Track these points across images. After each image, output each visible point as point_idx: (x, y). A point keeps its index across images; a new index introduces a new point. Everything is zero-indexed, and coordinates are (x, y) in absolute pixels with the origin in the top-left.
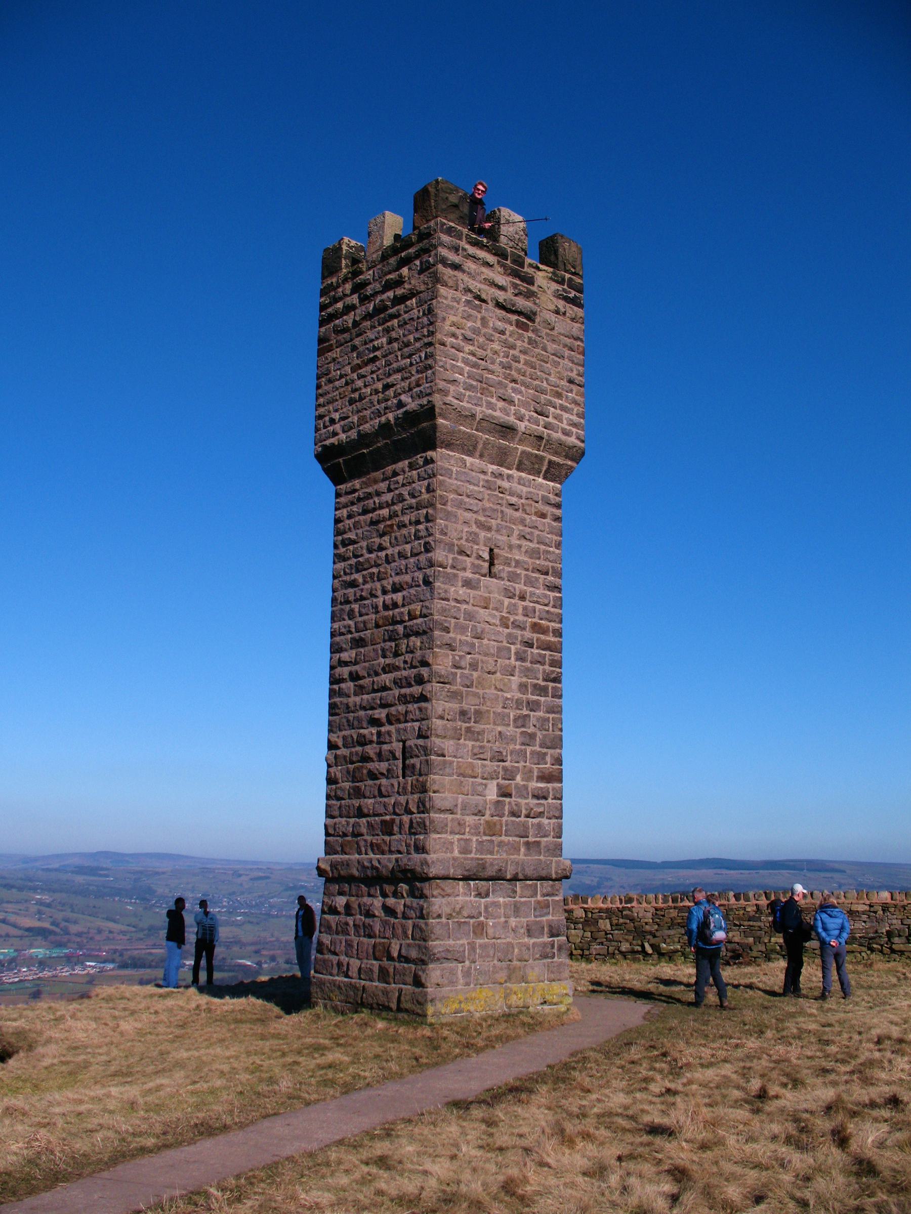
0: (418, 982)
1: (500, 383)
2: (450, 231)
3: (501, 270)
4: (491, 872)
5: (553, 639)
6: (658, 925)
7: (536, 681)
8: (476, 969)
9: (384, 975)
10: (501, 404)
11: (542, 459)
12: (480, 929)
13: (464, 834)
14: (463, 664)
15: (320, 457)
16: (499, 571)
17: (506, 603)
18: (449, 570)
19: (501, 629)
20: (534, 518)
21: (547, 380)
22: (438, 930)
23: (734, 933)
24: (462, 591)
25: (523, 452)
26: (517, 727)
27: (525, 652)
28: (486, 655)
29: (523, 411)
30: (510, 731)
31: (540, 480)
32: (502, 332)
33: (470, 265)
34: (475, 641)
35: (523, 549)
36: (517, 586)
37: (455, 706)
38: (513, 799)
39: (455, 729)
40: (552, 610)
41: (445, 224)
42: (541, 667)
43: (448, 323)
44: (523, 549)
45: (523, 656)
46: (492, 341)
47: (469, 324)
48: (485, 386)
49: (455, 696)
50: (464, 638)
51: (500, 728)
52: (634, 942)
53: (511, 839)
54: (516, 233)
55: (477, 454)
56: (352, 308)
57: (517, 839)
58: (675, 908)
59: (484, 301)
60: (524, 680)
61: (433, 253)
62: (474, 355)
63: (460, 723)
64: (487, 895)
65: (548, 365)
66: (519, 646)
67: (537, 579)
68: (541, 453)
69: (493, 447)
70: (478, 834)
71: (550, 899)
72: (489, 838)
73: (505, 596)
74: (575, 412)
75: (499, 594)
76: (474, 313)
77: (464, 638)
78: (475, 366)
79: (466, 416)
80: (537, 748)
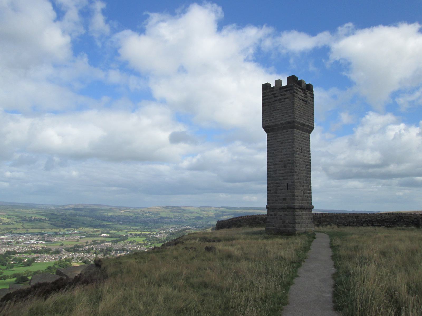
0: (294, 227)
2: (296, 86)
9: (285, 226)
10: (303, 120)
11: (308, 129)
12: (302, 218)
15: (263, 127)
18: (296, 152)
22: (297, 218)
24: (298, 156)
30: (304, 181)
31: (307, 134)
32: (303, 105)
33: (299, 93)
49: (297, 175)
78: (299, 113)
80: (308, 185)
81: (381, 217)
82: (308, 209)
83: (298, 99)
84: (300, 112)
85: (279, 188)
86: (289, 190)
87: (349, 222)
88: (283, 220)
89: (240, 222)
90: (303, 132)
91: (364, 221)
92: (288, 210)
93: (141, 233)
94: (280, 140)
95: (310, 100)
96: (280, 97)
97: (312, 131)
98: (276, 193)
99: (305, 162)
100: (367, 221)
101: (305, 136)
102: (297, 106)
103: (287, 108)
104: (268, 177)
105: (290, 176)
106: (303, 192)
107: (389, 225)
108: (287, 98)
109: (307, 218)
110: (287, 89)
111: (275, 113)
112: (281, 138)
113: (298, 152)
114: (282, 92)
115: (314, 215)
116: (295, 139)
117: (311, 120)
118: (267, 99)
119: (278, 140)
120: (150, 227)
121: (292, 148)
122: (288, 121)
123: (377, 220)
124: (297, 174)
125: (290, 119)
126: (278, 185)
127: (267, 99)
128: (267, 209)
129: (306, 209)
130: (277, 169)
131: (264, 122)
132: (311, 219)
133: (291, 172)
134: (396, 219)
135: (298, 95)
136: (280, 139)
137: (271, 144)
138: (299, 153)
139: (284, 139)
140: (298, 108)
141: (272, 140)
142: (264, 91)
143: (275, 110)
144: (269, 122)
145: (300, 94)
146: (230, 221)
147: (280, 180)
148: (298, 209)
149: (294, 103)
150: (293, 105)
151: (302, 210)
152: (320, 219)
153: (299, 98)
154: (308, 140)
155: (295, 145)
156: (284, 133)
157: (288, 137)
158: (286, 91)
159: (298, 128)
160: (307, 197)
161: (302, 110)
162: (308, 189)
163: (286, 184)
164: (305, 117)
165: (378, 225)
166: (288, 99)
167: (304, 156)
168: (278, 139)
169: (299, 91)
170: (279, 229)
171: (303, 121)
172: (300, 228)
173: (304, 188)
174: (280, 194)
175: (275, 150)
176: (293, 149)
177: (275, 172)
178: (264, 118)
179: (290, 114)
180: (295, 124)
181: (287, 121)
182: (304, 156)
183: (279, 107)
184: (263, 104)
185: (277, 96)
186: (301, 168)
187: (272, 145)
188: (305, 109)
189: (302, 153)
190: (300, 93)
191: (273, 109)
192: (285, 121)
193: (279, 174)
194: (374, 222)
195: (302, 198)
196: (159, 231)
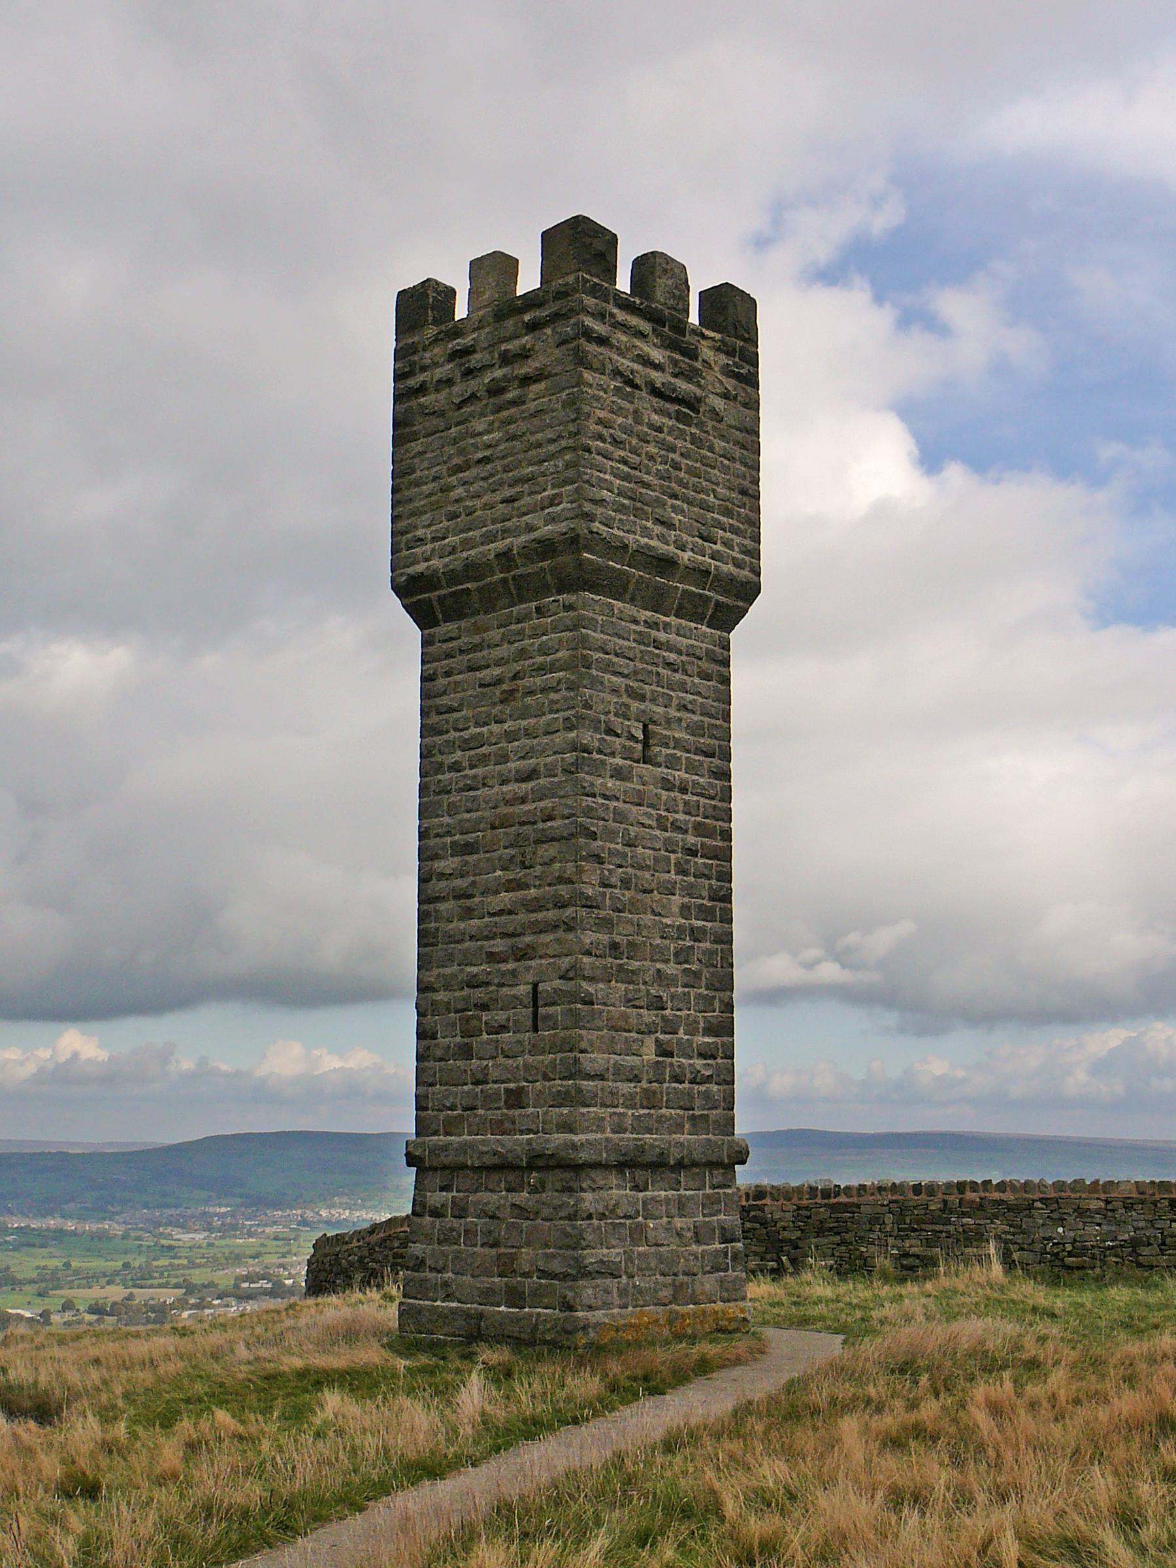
1: (657, 500)
4: (648, 1158)
5: (720, 844)
6: (802, 1231)
7: (701, 901)
8: (634, 1286)
9: (515, 1297)
10: (658, 529)
12: (638, 1234)
13: (617, 1107)
14: (613, 880)
15: (397, 589)
16: (656, 755)
17: (664, 798)
18: (595, 756)
19: (658, 833)
20: (697, 680)
21: (714, 491)
22: (589, 1237)
23: (913, 1242)
25: (685, 592)
26: (680, 963)
28: (641, 868)
29: (685, 537)
30: (671, 969)
32: (660, 430)
33: (622, 338)
34: (627, 849)
35: (684, 724)
36: (677, 773)
37: (604, 938)
38: (676, 1058)
39: (605, 967)
40: (719, 804)
41: (588, 281)
44: (684, 724)
45: (685, 867)
46: (648, 442)
47: (620, 420)
48: (639, 505)
49: (606, 924)
50: (613, 846)
51: (659, 966)
52: (768, 1257)
53: (673, 1112)
54: (676, 288)
56: (449, 382)
57: (681, 1112)
58: (825, 1205)
59: (637, 387)
60: (686, 900)
62: (625, 463)
63: (610, 960)
64: (646, 1189)
65: (716, 471)
66: (680, 855)
67: (701, 763)
68: (707, 593)
69: (647, 587)
70: (633, 1107)
71: (721, 1191)
72: (646, 1111)
73: (663, 788)
74: (748, 535)
76: (625, 404)
77: (613, 846)
78: (626, 478)
79: (616, 547)
80: (703, 991)
82: (695, 1164)
85: (485, 1016)
87: (1135, 1243)
88: (503, 1250)
93: (131, 1297)
94: (497, 671)
95: (726, 396)
96: (499, 373)
98: (466, 1052)
99: (677, 827)
102: (600, 428)
106: (657, 1040)
110: (543, 313)
112: (499, 662)
113: (613, 754)
118: (422, 389)
120: (185, 1262)
122: (537, 534)
125: (552, 519)
126: (479, 994)
127: (422, 389)
129: (680, 1165)
130: (474, 883)
136: (499, 662)
137: (445, 701)
139: (517, 667)
140: (616, 442)
146: (375, 1238)
147: (492, 957)
148: (597, 1165)
149: (578, 411)
151: (640, 1175)
158: (534, 327)
159: (617, 587)
161: (651, 458)
163: (523, 990)
169: (624, 327)
171: (662, 538)
173: (667, 1012)
175: (466, 745)
176: (573, 735)
179: (554, 486)
181: (532, 536)
187: (451, 710)
196: (236, 1286)
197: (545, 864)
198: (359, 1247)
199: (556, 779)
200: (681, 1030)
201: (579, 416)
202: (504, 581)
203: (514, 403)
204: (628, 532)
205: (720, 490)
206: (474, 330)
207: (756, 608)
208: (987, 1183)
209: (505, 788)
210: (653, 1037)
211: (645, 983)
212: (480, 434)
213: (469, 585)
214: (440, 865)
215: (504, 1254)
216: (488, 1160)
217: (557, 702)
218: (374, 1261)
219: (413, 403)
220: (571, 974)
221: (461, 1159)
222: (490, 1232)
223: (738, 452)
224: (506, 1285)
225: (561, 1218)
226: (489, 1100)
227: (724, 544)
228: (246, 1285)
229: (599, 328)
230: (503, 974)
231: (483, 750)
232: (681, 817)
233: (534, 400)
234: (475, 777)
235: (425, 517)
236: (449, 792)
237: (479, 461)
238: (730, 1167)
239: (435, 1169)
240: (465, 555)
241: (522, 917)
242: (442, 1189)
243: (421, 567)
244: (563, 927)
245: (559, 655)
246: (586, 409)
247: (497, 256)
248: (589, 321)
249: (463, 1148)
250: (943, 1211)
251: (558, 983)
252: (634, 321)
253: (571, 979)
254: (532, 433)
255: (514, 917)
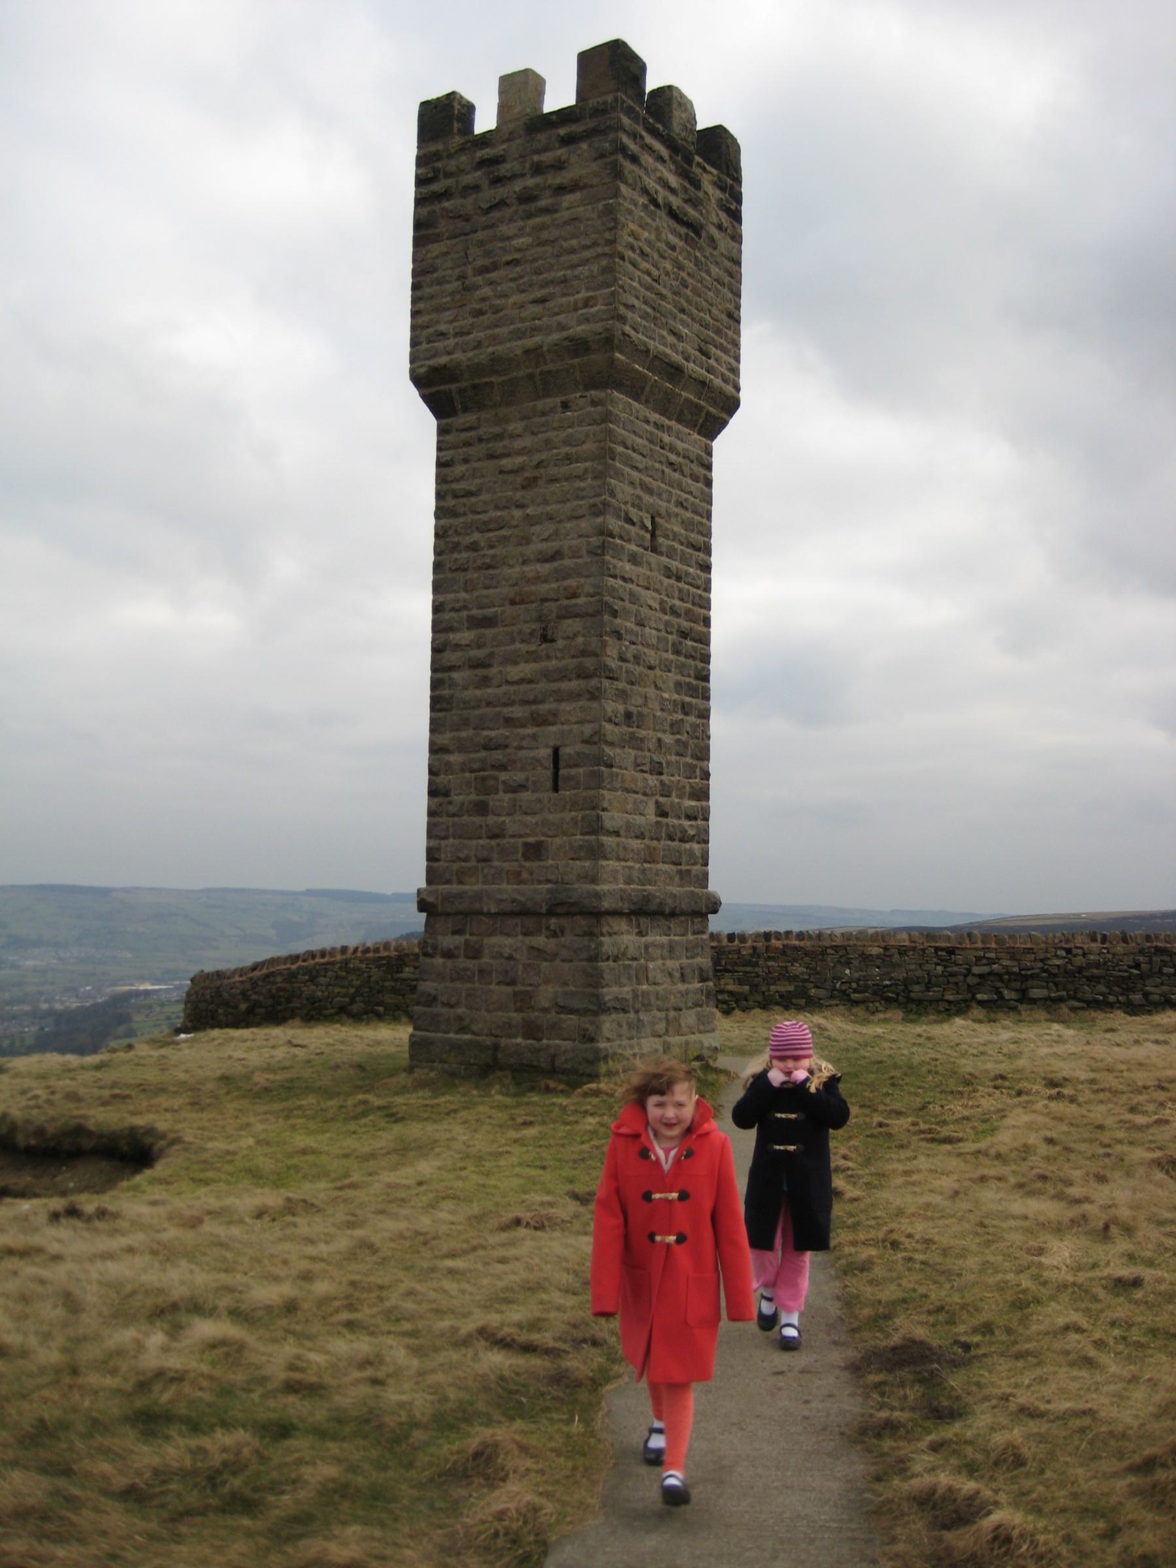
3: (672, 167)
9: (531, 1030)
10: (671, 339)
11: (699, 408)
12: (642, 975)
15: (419, 380)
18: (618, 541)
19: (661, 615)
20: (690, 481)
22: (608, 976)
24: (628, 567)
25: (686, 400)
27: (681, 643)
30: (668, 739)
31: (696, 436)
32: (673, 248)
33: (647, 159)
42: (693, 663)
43: (626, 231)
49: (623, 695)
51: (660, 735)
55: (643, 398)
61: (611, 137)
62: (649, 274)
75: (659, 570)
78: (649, 288)
80: (689, 760)
81: (1069, 951)
82: (682, 913)
83: (643, 200)
84: (655, 284)
85: (503, 776)
86: (566, 793)
87: (906, 982)
88: (519, 988)
89: (312, 980)
90: (667, 422)
91: (981, 976)
92: (553, 921)
94: (519, 460)
95: (720, 227)
96: (530, 182)
97: (724, 424)
98: (482, 809)
99: (674, 612)
100: (999, 976)
101: (680, 446)
102: (631, 240)
103: (573, 251)
104: (437, 703)
105: (575, 696)
106: (657, 802)
107: (1103, 994)
108: (574, 187)
109: (677, 975)
111: (491, 283)
112: (520, 452)
113: (629, 541)
114: (538, 152)
115: (725, 942)
116: (613, 459)
117: (725, 350)
118: (446, 194)
119: (506, 463)
121: (598, 510)
122: (571, 332)
123: (1045, 971)
124: (621, 685)
126: (497, 756)
127: (446, 194)
128: (425, 914)
129: (673, 914)
130: (491, 655)
131: (425, 346)
132: (703, 979)
133: (583, 674)
134: (1137, 966)
135: (647, 174)
136: (520, 452)
138: (642, 550)
139: (543, 456)
140: (643, 254)
141: (466, 461)
142: (433, 147)
143: (495, 267)
144: (451, 342)
145: (659, 172)
146: (257, 973)
147: (509, 722)
149: (615, 220)
150: (610, 229)
151: (644, 922)
152: (756, 964)
153: (652, 192)
154: (696, 479)
155: (612, 494)
156: (543, 414)
157: (567, 442)
159: (636, 388)
160: (682, 840)
161: (667, 274)
162: (688, 789)
163: (545, 752)
164: (683, 322)
165: (1053, 995)
166: (578, 195)
167: (668, 572)
168: (508, 455)
169: (649, 148)
170: (496, 1047)
171: (673, 347)
172: (631, 1038)
173: (664, 777)
174: (507, 819)
175: (485, 528)
176: (599, 520)
177: (481, 672)
178: (421, 320)
179: (588, 289)
180: (618, 355)
181: (565, 334)
182: (669, 577)
183: (518, 242)
184: (419, 225)
185: (514, 177)
186: (651, 653)
187: (469, 494)
188: (683, 274)
189: (661, 554)
190: (659, 166)
191: (480, 262)
192: (556, 337)
193: (504, 688)
194: (1030, 983)
195: (647, 841)
197: (568, 638)
198: (242, 982)
199: (580, 561)
200: (674, 795)
201: (615, 225)
202: (531, 377)
203: (546, 211)
204: (650, 338)
205: (714, 311)
206: (503, 142)
207: (735, 422)
208: (788, 933)
209: (526, 568)
210: (654, 799)
211: (649, 750)
212: (509, 238)
213: (493, 379)
214: (454, 637)
215: (522, 992)
216: (507, 907)
217: (583, 489)
218: (256, 993)
219: (437, 207)
220: (596, 739)
221: (477, 906)
222: (506, 972)
223: (727, 279)
224: (523, 1019)
225: (581, 960)
226: (504, 853)
227: (716, 360)
228: (8, 1008)
229: (633, 147)
230: (523, 738)
231: (503, 532)
232: (677, 603)
233: (568, 209)
234: (494, 556)
235: (448, 313)
236: (465, 570)
237: (508, 263)
238: (706, 915)
239: (448, 914)
240: (491, 349)
241: (543, 685)
242: (454, 933)
243: (443, 360)
244: (587, 696)
245: (586, 447)
246: (622, 219)
247: (527, 73)
248: (625, 139)
249: (478, 897)
250: (752, 955)
251: (579, 747)
252: (657, 145)
253: (595, 743)
254: (566, 240)
255: (534, 686)
